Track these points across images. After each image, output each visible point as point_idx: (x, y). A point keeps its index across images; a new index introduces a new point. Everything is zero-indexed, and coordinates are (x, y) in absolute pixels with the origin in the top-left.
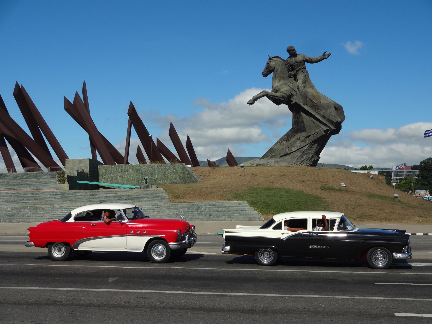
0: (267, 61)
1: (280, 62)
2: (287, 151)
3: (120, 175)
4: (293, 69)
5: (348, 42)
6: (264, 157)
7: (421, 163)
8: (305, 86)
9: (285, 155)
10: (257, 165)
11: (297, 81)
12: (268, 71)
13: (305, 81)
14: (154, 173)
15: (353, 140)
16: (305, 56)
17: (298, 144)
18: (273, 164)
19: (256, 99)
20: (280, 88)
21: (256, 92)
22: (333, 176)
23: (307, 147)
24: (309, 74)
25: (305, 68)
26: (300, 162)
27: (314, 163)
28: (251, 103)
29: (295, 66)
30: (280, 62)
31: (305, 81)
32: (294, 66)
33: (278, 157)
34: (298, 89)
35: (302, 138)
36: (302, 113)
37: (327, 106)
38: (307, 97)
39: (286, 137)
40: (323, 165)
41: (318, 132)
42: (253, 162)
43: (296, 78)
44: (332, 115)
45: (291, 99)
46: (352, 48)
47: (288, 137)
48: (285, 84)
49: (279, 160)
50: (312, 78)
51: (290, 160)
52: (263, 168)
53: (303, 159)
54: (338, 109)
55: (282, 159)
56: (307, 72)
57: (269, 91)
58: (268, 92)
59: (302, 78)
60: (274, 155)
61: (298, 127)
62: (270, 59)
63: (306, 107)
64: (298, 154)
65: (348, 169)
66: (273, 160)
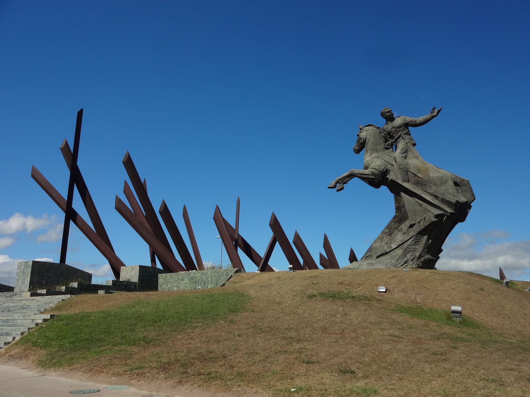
2: (386, 249)
3: (176, 284)
8: (405, 158)
9: (382, 255)
14: (207, 281)
19: (344, 181)
20: (370, 163)
23: (411, 240)
26: (402, 264)
30: (373, 130)
33: (375, 258)
34: (395, 161)
38: (408, 171)
39: (387, 230)
44: (449, 193)
48: (377, 157)
49: (373, 262)
53: (405, 259)
55: (378, 259)
63: (406, 185)
64: (399, 252)
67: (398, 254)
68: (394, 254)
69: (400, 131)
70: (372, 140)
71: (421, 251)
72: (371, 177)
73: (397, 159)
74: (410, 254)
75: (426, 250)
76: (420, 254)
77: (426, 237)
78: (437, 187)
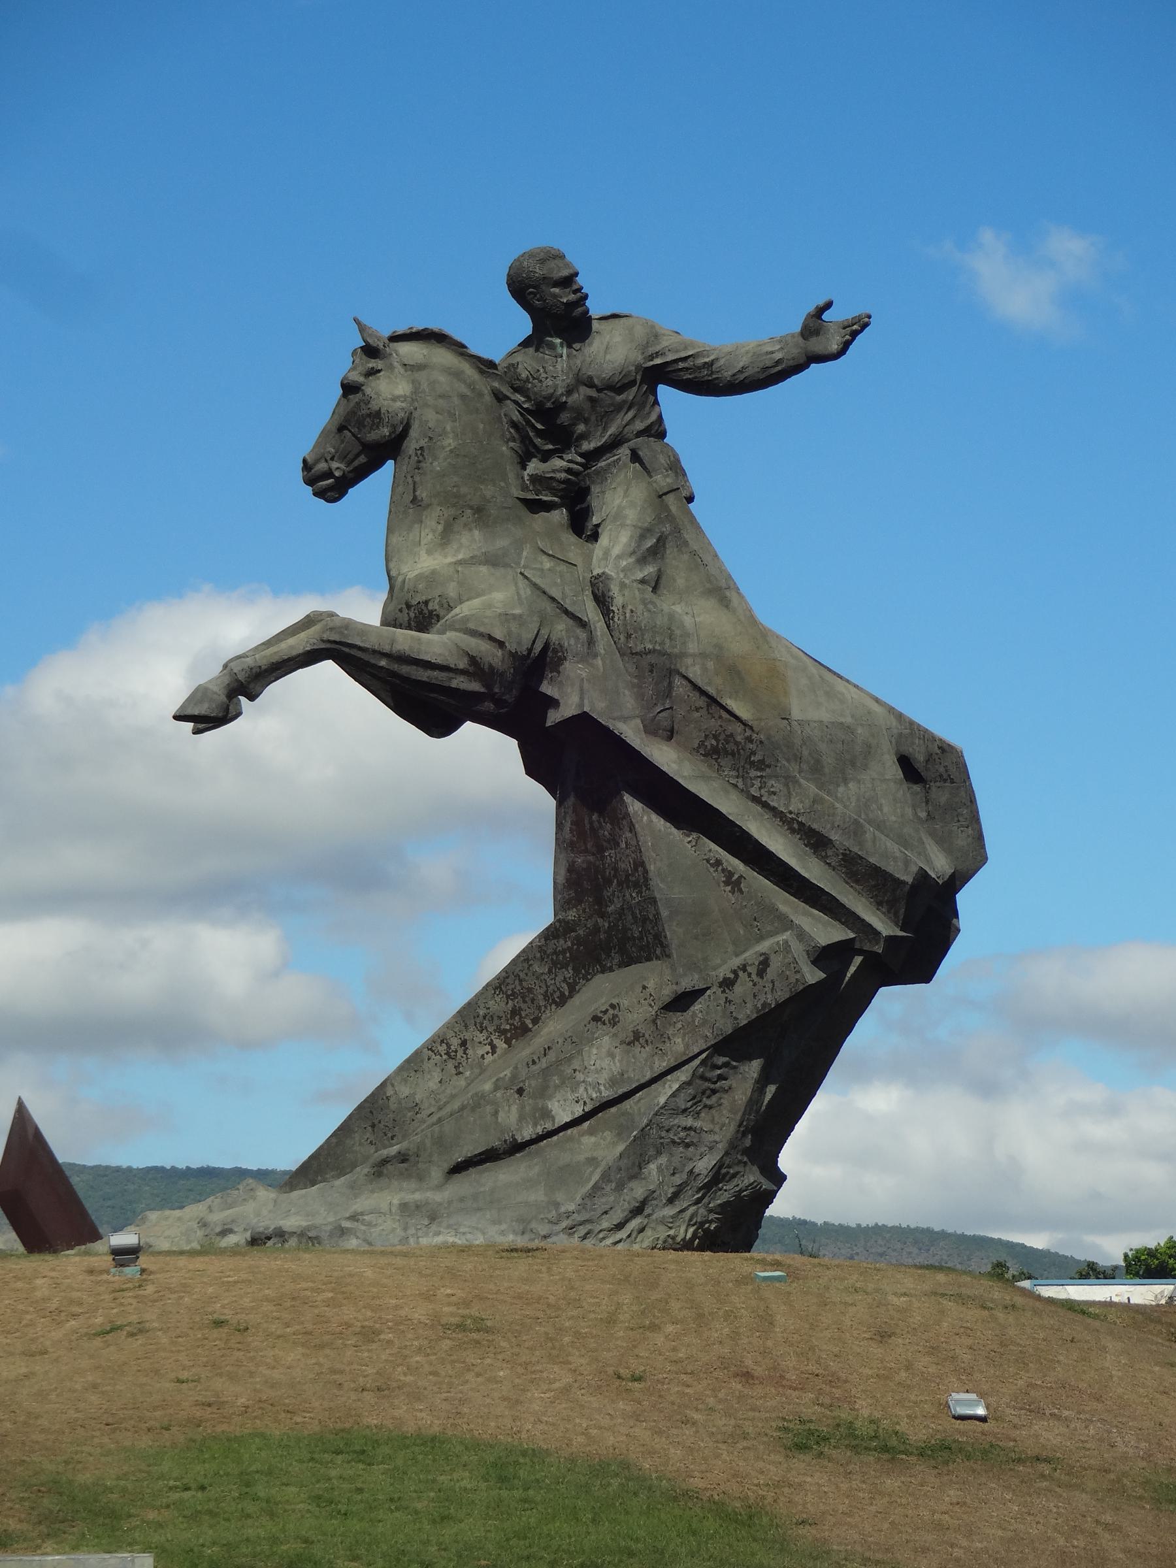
0: (340, 362)
1: (458, 375)
2: (513, 1120)
4: (563, 439)
5: (987, 236)
6: (313, 1171)
7: (173, 1167)
9: (490, 1156)
10: (256, 1241)
11: (594, 537)
12: (356, 448)
13: (661, 541)
15: (1039, 1027)
16: (654, 335)
17: (603, 1064)
18: (387, 1230)
19: (248, 681)
20: (452, 591)
21: (244, 626)
22: (883, 1336)
23: (672, 1084)
24: (696, 481)
25: (657, 431)
26: (617, 1216)
27: (737, 1223)
28: (209, 713)
29: (579, 417)
30: (458, 375)
31: (661, 541)
32: (572, 414)
33: (436, 1174)
34: (602, 601)
35: (637, 1014)
36: (634, 806)
37: (845, 752)
38: (672, 672)
39: (498, 1005)
40: (804, 1235)
41: (764, 964)
42: (218, 1218)
43: (587, 513)
44: (880, 826)
45: (546, 688)
46: (1020, 286)
47: (514, 1004)
48: (493, 561)
49: (438, 1197)
50: (721, 518)
51: (538, 1196)
52: (307, 1263)
53: (638, 1191)
54: (932, 772)
56: (675, 467)
57: (364, 609)
58: (348, 624)
59: (631, 515)
60: (403, 1158)
61: (600, 922)
62: (370, 351)
63: (665, 757)
64: (601, 1146)
65: (1011, 1267)
66: (388, 1197)
67: (592, 1161)
68: (565, 1158)
69: (618, 408)
70: (450, 442)
71: (721, 1147)
72: (460, 683)
73: (615, 590)
74: (663, 1160)
75: (748, 1142)
76: (720, 1165)
77: (754, 1067)
78: (821, 787)
